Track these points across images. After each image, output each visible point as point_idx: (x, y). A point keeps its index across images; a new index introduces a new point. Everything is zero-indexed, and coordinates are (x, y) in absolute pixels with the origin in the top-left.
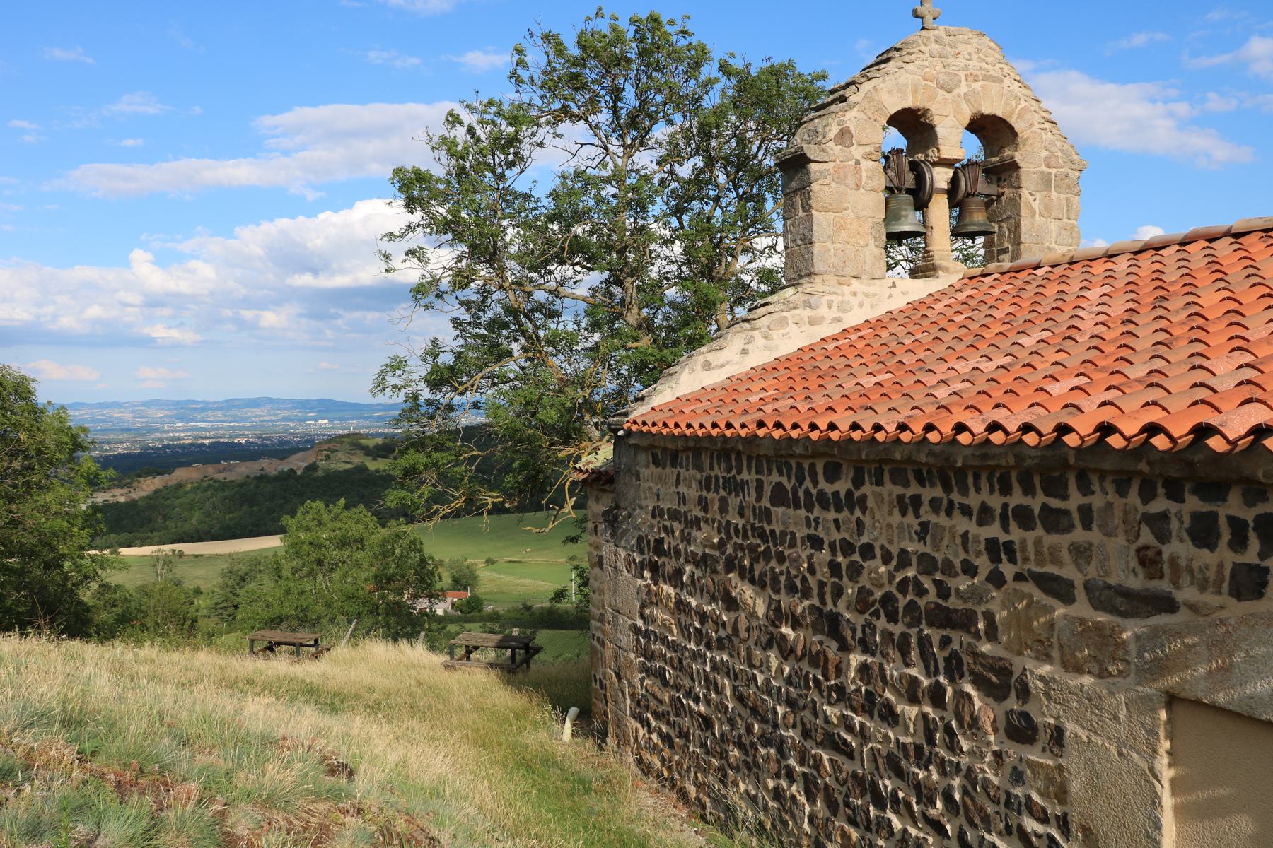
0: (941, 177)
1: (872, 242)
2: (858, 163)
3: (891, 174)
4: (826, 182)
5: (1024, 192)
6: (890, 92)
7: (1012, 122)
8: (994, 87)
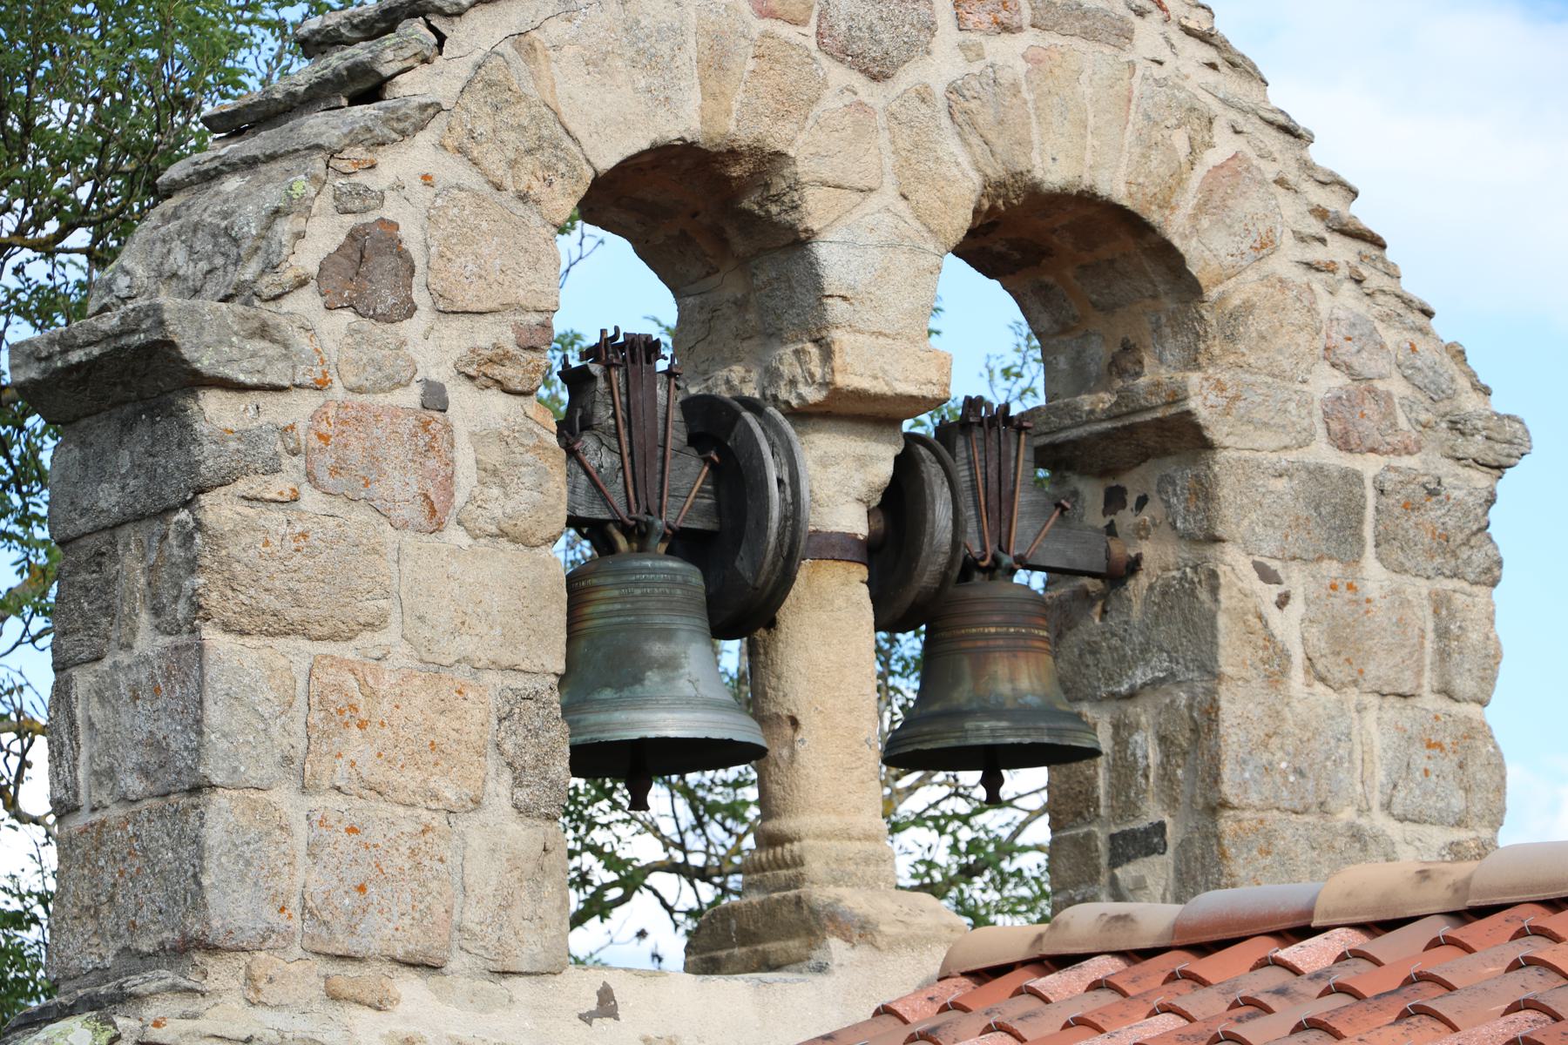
0: (838, 481)
1: (500, 790)
2: (435, 399)
3: (599, 456)
4: (278, 486)
5: (1234, 564)
6: (595, 63)
7: (1176, 227)
8: (1093, 58)
